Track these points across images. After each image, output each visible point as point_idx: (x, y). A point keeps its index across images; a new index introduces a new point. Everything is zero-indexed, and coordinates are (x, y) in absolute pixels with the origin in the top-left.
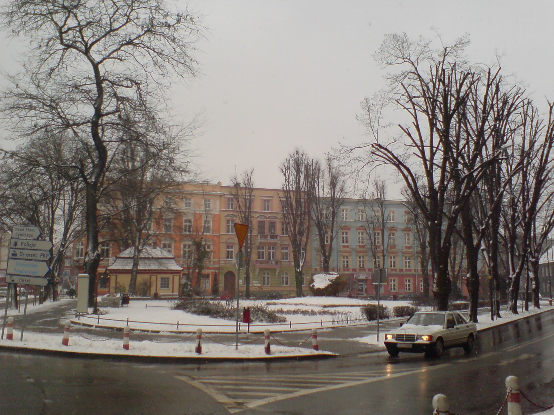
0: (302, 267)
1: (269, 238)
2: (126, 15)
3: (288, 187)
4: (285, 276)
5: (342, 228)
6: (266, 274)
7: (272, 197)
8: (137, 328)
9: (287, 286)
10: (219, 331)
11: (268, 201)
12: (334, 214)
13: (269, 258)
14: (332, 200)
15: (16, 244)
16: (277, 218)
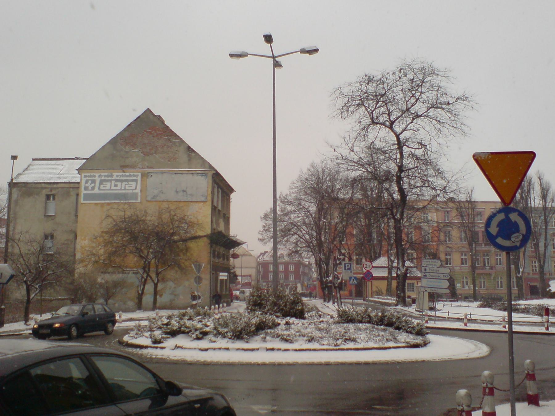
0: (522, 272)
1: (483, 246)
4: (500, 280)
6: (499, 278)
7: (484, 209)
8: (478, 319)
9: (502, 289)
10: (530, 321)
13: (485, 264)
14: (543, 209)
15: (425, 270)
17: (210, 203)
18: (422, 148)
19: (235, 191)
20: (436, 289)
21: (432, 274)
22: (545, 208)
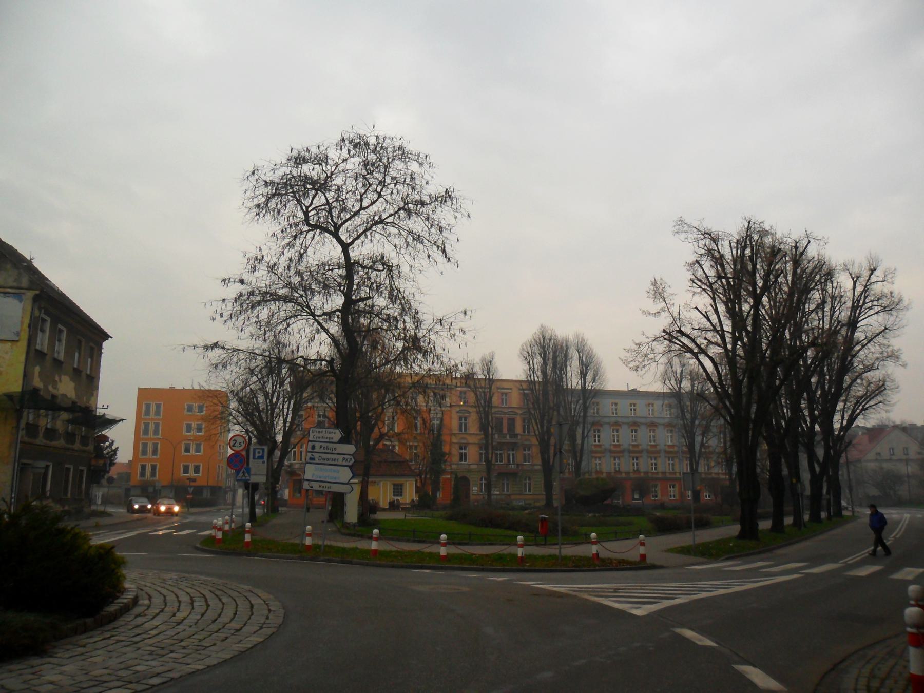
2: (376, 191)
3: (532, 378)
5: (593, 424)
7: (511, 389)
11: (506, 394)
12: (585, 408)
15: (313, 447)
16: (516, 414)
17: (23, 344)
18: (384, 269)
19: (112, 338)
20: (328, 485)
21: (324, 456)
22: (584, 389)
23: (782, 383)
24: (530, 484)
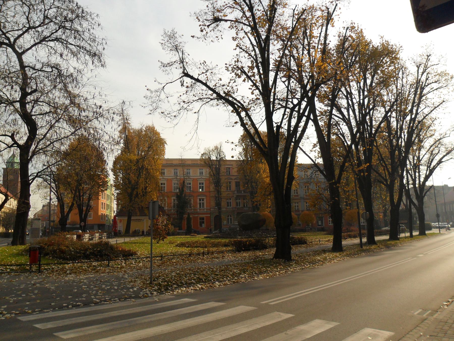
23: (416, 128)
24: (231, 219)
